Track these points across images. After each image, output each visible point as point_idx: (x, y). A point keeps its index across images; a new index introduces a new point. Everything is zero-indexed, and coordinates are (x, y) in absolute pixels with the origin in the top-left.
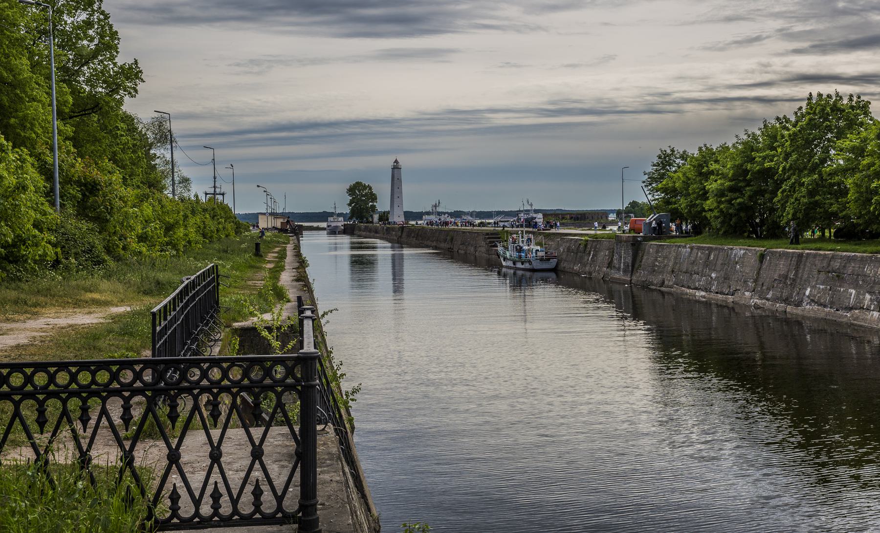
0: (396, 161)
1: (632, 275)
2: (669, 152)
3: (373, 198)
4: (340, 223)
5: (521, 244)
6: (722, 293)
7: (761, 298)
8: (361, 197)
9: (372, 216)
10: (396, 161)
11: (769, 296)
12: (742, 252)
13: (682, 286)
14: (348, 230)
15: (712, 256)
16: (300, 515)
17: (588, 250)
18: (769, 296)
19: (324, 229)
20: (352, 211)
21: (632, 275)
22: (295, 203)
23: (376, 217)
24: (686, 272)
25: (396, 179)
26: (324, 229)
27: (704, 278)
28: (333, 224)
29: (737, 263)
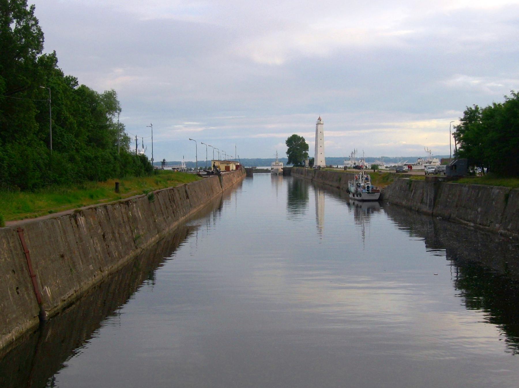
0: (319, 119)
1: (433, 209)
2: (473, 108)
3: (306, 147)
4: (280, 167)
5: (360, 182)
6: (483, 225)
7: (504, 229)
8: (296, 145)
9: (304, 162)
10: (319, 119)
11: (509, 227)
12: (498, 190)
13: (461, 218)
14: (286, 173)
15: (480, 194)
16: (2, 305)
17: (411, 188)
18: (509, 227)
19: (267, 171)
20: (290, 158)
21: (433, 209)
22: (247, 154)
23: (307, 162)
24: (464, 207)
25: (319, 132)
26: (267, 171)
27: (473, 212)
28: (275, 168)
29: (493, 200)
